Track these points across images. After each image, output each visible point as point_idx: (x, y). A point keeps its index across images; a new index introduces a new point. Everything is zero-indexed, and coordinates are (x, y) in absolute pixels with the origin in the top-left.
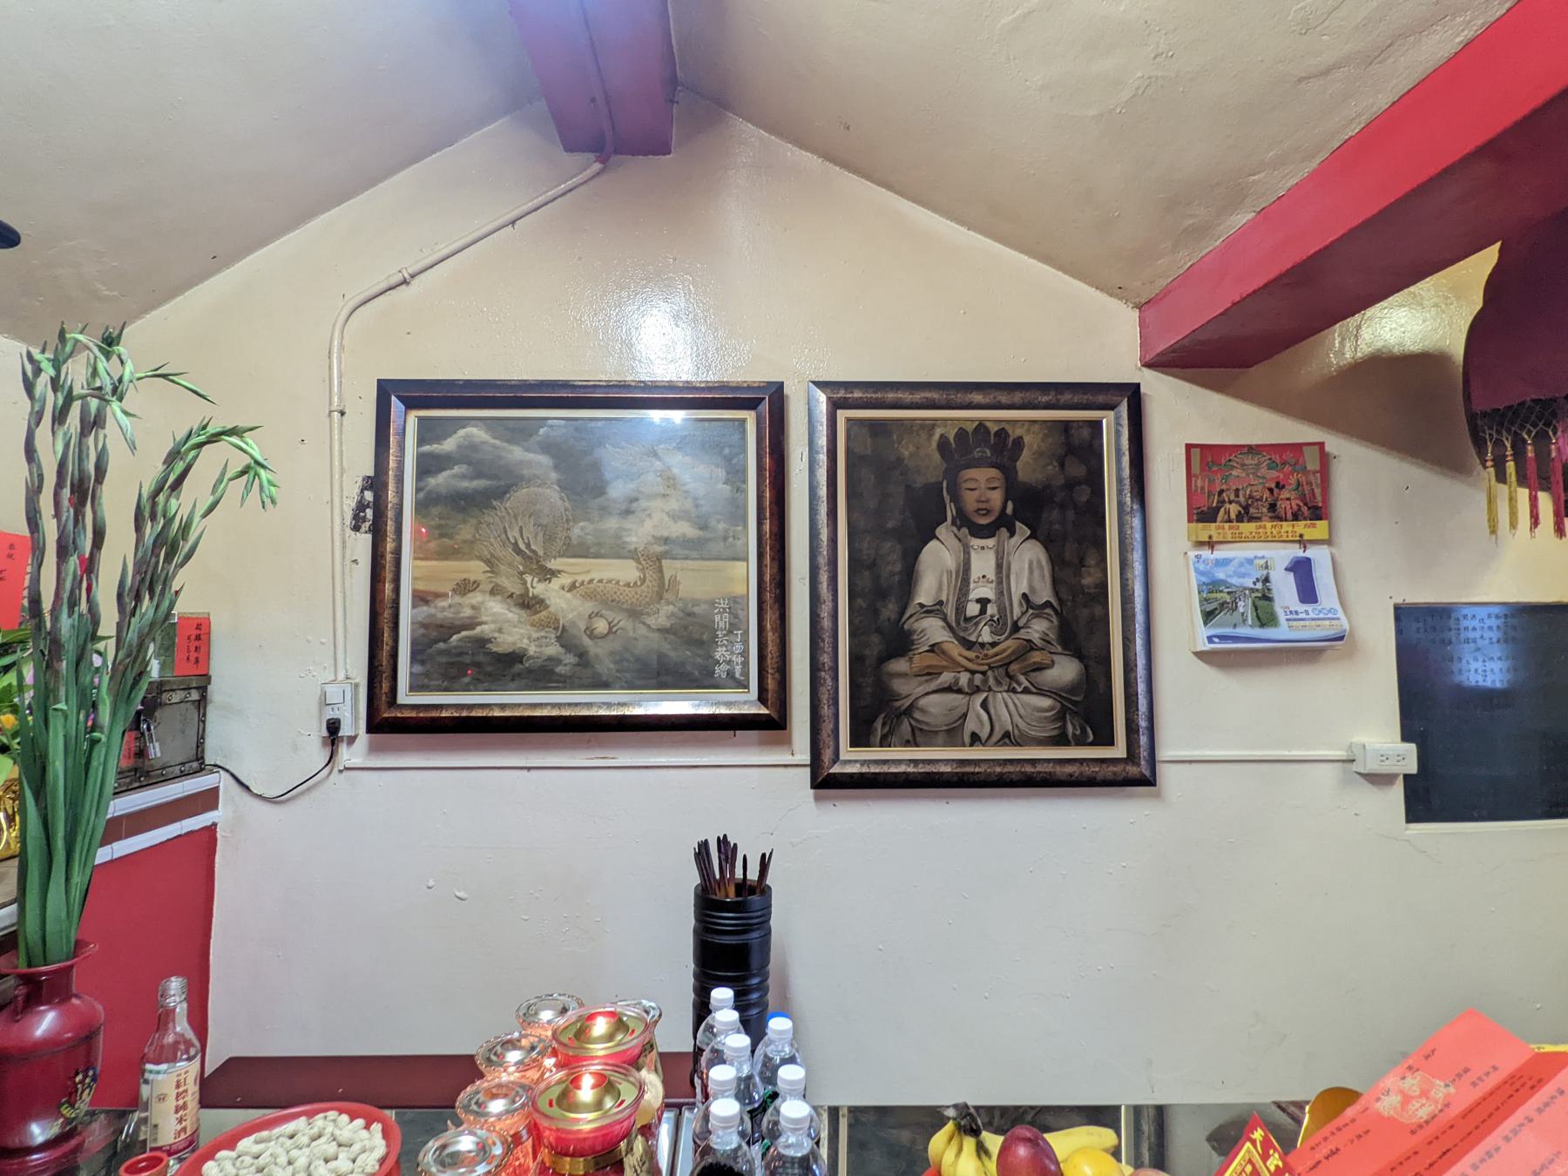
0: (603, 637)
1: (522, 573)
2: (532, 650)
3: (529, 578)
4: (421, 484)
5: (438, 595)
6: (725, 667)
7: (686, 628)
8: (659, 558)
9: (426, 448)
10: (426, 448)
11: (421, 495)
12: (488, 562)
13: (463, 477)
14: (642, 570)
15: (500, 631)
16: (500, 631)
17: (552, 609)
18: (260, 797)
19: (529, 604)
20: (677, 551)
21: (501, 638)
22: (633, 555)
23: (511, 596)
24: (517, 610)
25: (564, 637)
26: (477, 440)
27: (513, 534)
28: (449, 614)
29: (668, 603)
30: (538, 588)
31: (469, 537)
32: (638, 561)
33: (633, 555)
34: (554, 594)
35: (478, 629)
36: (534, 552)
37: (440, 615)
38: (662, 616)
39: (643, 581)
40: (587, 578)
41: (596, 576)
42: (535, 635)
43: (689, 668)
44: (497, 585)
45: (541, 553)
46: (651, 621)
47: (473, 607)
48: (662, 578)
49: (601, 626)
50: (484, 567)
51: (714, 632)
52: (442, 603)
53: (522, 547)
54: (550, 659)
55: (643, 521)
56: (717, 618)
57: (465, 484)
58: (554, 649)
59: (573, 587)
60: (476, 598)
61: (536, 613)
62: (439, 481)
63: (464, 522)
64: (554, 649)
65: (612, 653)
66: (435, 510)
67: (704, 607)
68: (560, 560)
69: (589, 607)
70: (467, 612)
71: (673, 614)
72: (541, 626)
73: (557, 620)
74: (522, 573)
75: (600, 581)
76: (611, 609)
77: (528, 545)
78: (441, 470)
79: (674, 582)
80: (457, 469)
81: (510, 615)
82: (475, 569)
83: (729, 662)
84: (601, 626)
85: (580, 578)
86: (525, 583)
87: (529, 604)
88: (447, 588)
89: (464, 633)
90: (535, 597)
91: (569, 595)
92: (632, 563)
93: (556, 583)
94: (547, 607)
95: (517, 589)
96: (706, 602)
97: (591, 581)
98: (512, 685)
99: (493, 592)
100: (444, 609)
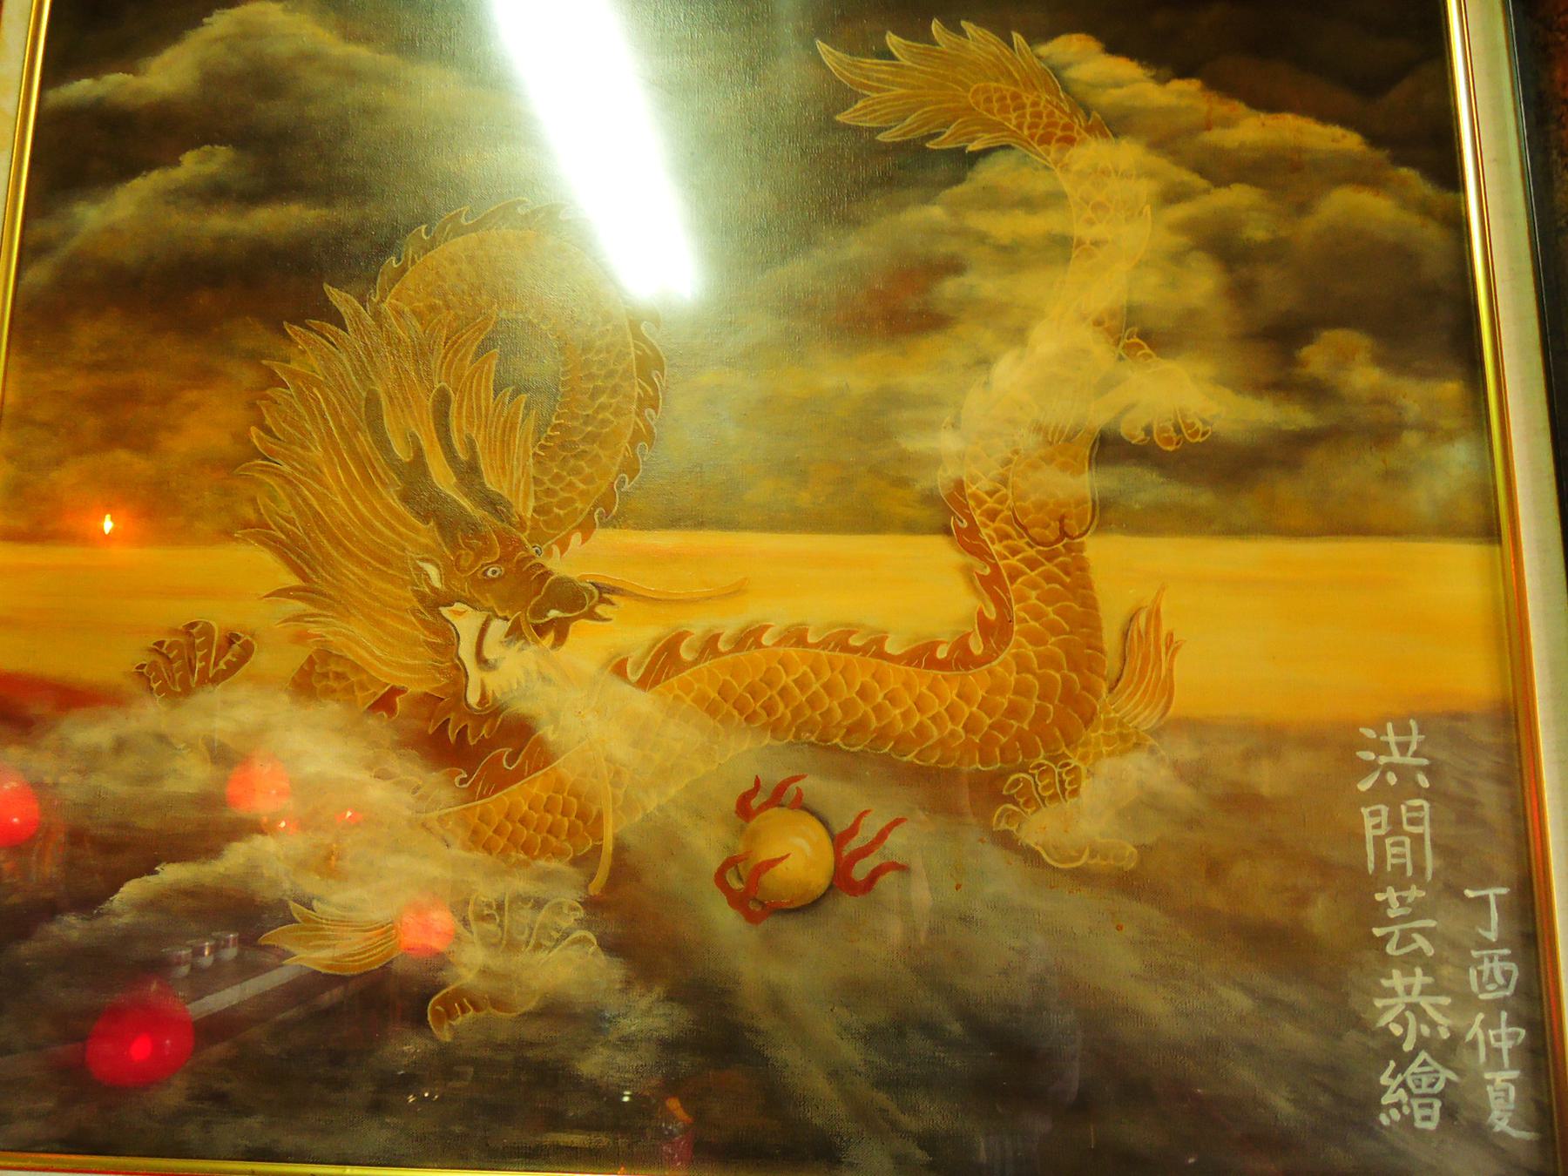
0: (809, 907)
1: (434, 603)
2: (471, 962)
3: (466, 622)
4: (46, 229)
5: (74, 697)
6: (1425, 1073)
7: (1215, 870)
8: (1058, 537)
9: (81, 89)
10: (81, 89)
11: (40, 274)
12: (290, 550)
13: (214, 193)
14: (992, 585)
15: (327, 864)
16: (327, 864)
17: (566, 767)
18: (813, 813)
19: (469, 743)
20: (1149, 487)
21: (335, 899)
22: (948, 515)
23: (385, 703)
24: (412, 771)
25: (629, 913)
26: (282, 49)
27: (407, 427)
28: (112, 784)
29: (1127, 741)
30: (510, 671)
31: (221, 441)
32: (970, 542)
33: (948, 515)
34: (581, 700)
35: (235, 857)
36: (492, 503)
37: (72, 787)
38: (1099, 803)
39: (996, 631)
40: (729, 623)
41: (776, 613)
42: (486, 892)
43: (1245, 1075)
44: (325, 655)
45: (525, 508)
46: (1038, 828)
47: (221, 755)
48: (1087, 617)
49: (799, 854)
50: (272, 570)
51: (1358, 887)
52: (90, 733)
53: (442, 477)
54: (554, 1010)
55: (984, 362)
56: (1372, 822)
57: (221, 222)
58: (569, 965)
59: (663, 663)
60: (228, 711)
61: (501, 781)
62: (117, 214)
63: (204, 376)
64: (569, 965)
65: (854, 991)
66: (87, 334)
67: (1299, 763)
68: (604, 537)
69: (744, 756)
70: (191, 775)
71: (1151, 802)
72: (503, 842)
73: (589, 821)
74: (434, 603)
75: (796, 636)
76: (847, 775)
77: (469, 473)
78: (128, 170)
79: (1146, 640)
80: (193, 165)
81: (377, 792)
82: (234, 580)
83: (1448, 1050)
84: (799, 854)
85: (698, 624)
86: (447, 639)
87: (469, 743)
88: (106, 664)
89: (172, 874)
90: (492, 710)
91: (645, 703)
92: (940, 553)
93: (588, 645)
94: (543, 757)
95: (412, 675)
96: (1313, 739)
97: (749, 638)
98: (376, 1135)
99: (310, 682)
100: (91, 760)
